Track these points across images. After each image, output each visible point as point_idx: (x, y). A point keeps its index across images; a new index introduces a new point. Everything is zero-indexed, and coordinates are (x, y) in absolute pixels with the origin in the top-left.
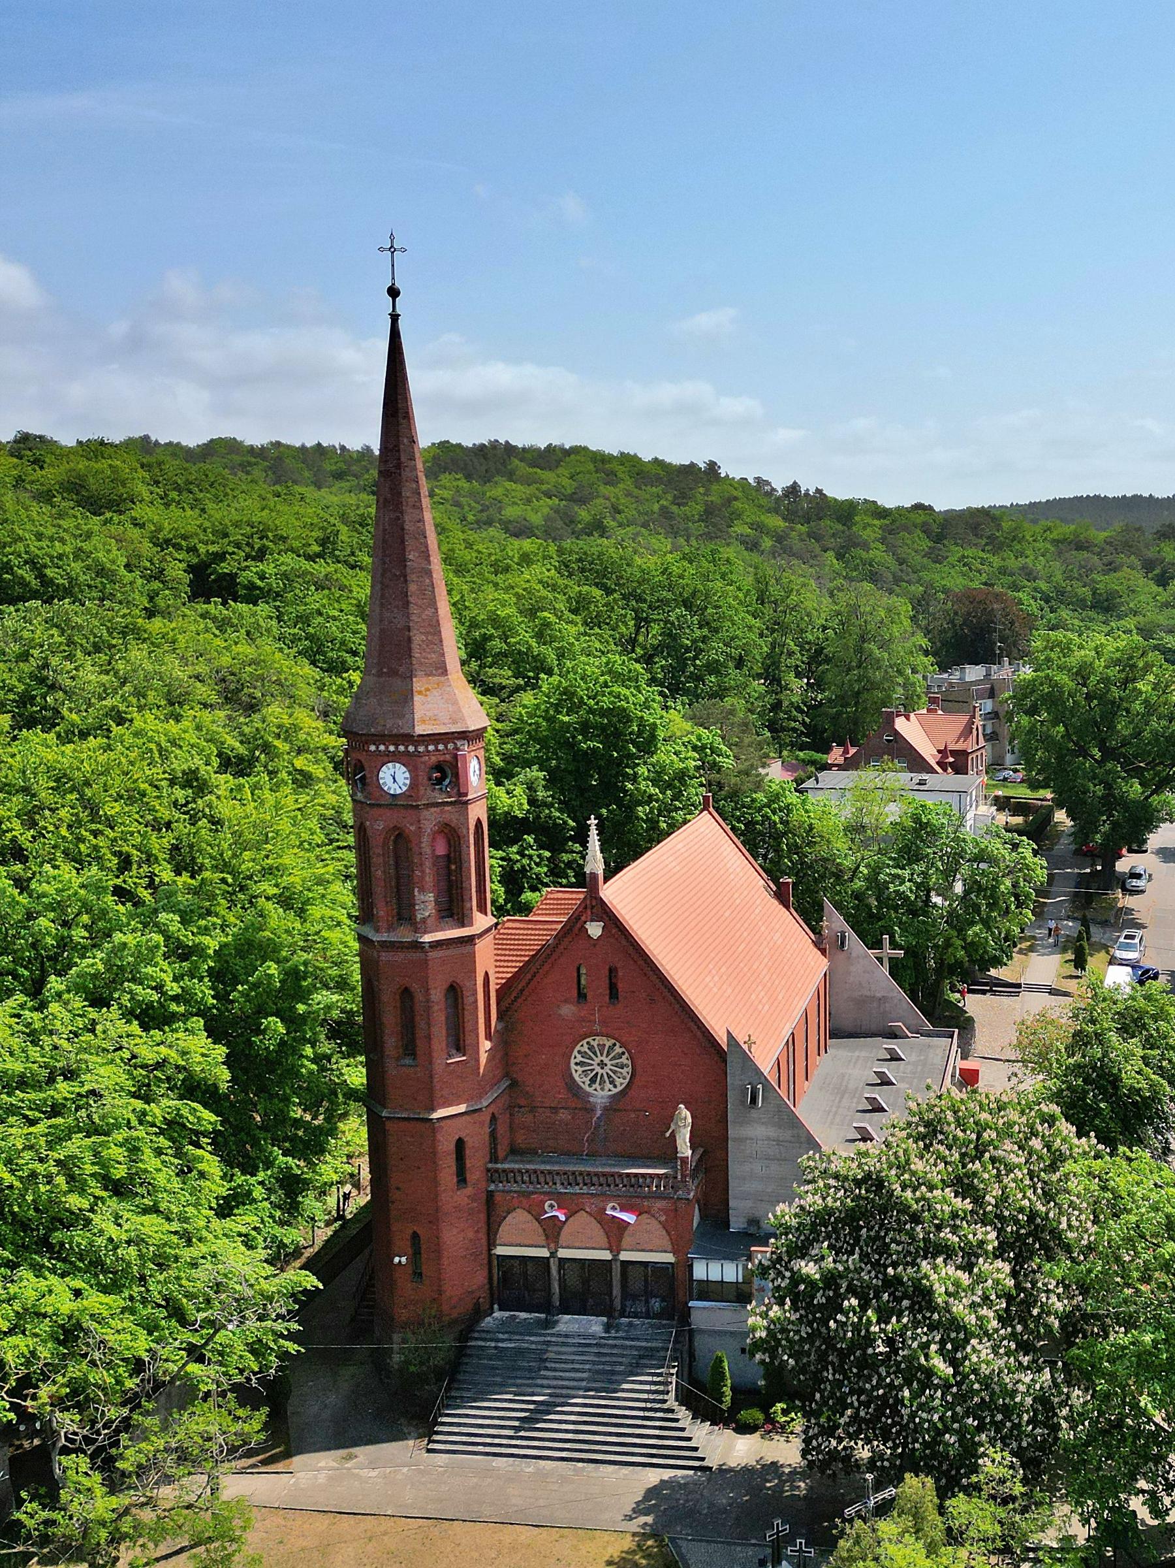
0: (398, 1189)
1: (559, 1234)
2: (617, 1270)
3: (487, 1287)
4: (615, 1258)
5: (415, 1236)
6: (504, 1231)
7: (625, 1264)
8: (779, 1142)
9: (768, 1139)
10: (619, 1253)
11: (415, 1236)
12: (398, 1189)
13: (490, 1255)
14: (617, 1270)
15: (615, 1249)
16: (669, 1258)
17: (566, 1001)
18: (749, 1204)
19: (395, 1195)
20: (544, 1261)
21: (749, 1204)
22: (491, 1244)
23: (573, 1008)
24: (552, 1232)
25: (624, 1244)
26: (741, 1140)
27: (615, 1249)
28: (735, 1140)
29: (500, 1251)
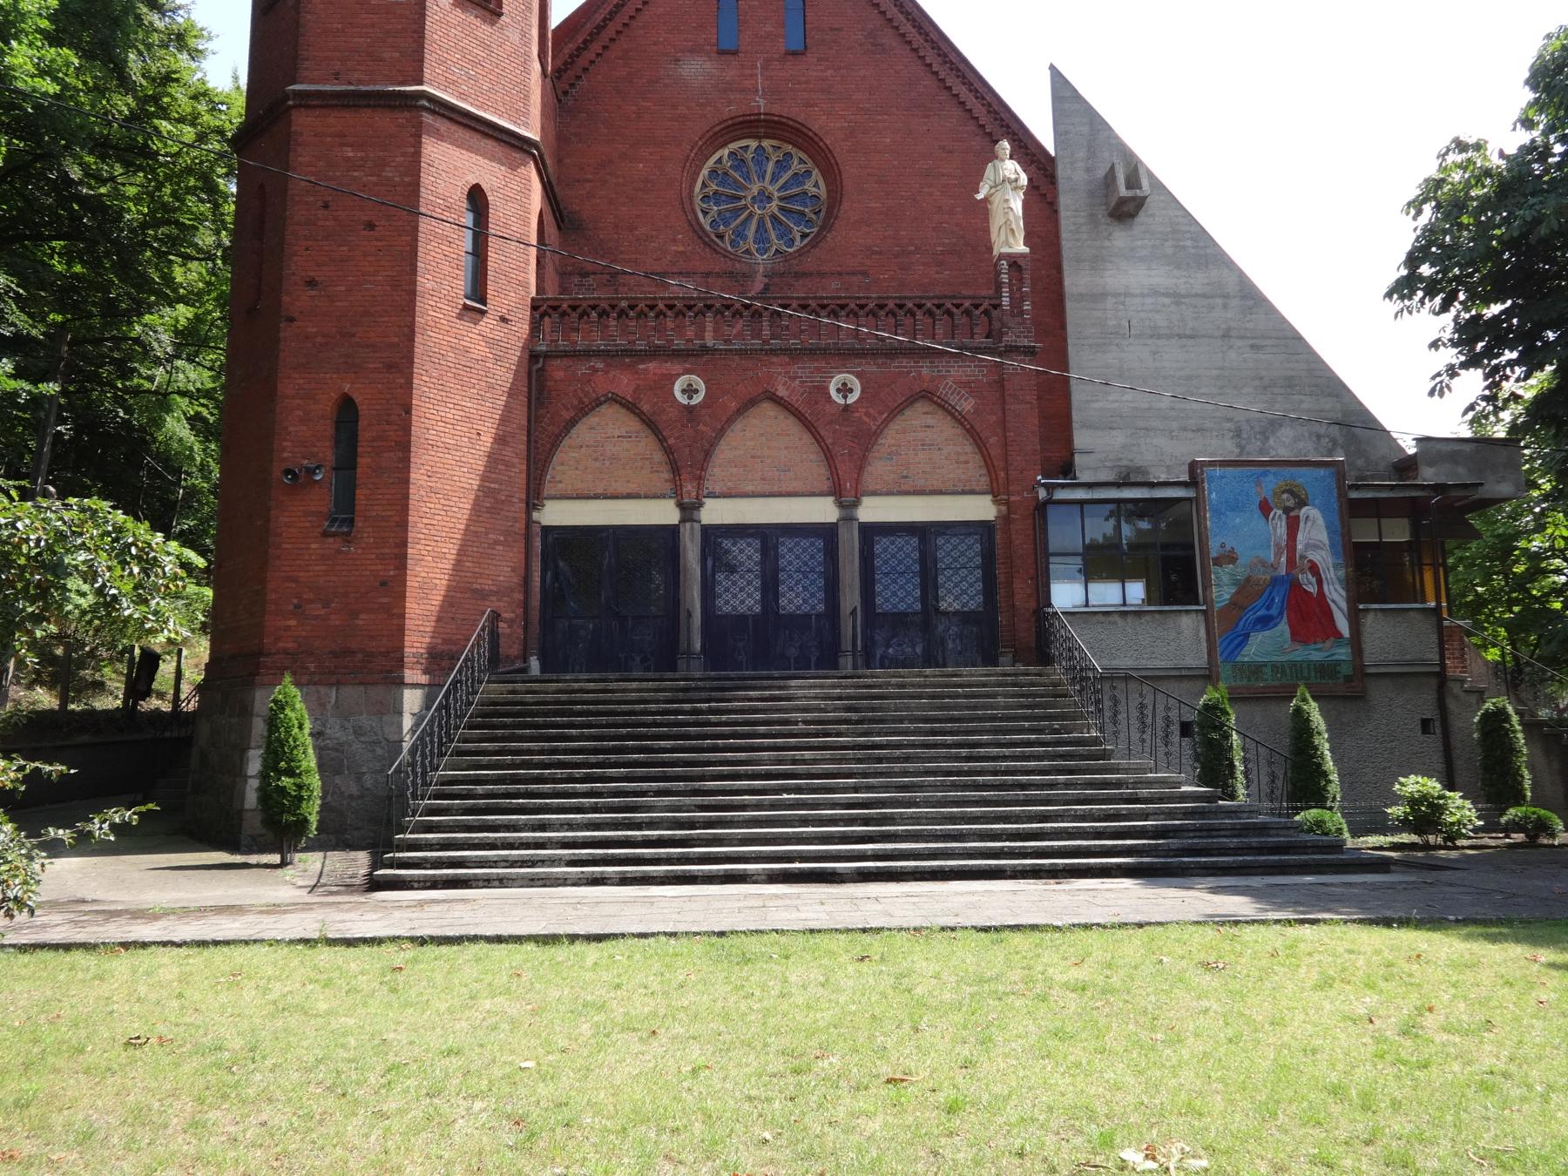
0: (311, 283)
1: (708, 454)
2: (850, 545)
3: (519, 596)
4: (848, 518)
5: (347, 409)
6: (566, 464)
7: (871, 531)
8: (1177, 297)
9: (1155, 293)
10: (856, 504)
11: (347, 409)
12: (311, 283)
13: (529, 522)
14: (850, 545)
15: (846, 494)
16: (981, 508)
17: (695, 50)
18: (1118, 439)
19: (298, 299)
20: (669, 534)
21: (1118, 439)
22: (534, 497)
23: (708, 65)
24: (686, 459)
25: (869, 480)
26: (1099, 297)
27: (846, 494)
28: (1081, 297)
29: (556, 514)
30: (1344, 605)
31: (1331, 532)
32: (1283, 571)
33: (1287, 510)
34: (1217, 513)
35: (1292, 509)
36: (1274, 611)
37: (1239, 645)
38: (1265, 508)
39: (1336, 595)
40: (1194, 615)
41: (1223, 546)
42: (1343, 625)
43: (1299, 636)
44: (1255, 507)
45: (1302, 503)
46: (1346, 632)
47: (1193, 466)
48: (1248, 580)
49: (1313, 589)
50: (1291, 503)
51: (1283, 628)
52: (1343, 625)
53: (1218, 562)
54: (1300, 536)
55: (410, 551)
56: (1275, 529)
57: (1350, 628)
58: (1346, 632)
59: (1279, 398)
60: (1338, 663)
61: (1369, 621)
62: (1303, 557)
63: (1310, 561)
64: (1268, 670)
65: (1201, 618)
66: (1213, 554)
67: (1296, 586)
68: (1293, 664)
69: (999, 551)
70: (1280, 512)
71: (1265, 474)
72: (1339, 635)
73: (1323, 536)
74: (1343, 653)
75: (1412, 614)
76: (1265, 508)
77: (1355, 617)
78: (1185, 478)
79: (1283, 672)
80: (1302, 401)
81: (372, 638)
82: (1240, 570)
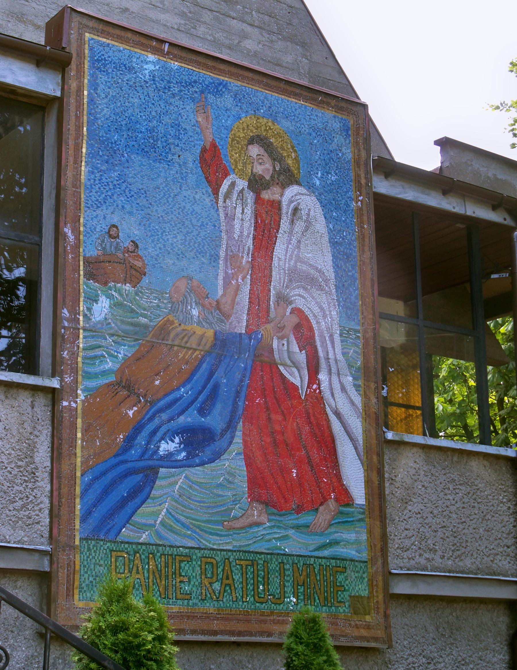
30: (357, 425)
31: (340, 257)
32: (240, 323)
33: (256, 184)
34: (107, 151)
35: (267, 186)
36: (215, 420)
37: (133, 493)
38: (213, 165)
39: (345, 403)
40: (24, 399)
41: (112, 232)
42: (354, 475)
43: (266, 489)
44: (191, 158)
45: (287, 177)
46: (359, 493)
47: (56, 27)
48: (163, 330)
49: (297, 378)
50: (264, 168)
51: (233, 463)
52: (354, 475)
53: (97, 270)
54: (280, 249)
55: (364, 492)
56: (230, 218)
57: (368, 482)
58: (359, 493)
59: (207, 16)
60: (341, 564)
61: (406, 468)
62: (283, 299)
63: (298, 312)
64: (192, 570)
65: (41, 408)
66: (90, 250)
67: (266, 366)
68: (250, 560)
69: (271, 552)
70: (242, 184)
71: (218, 89)
72: (344, 497)
73: (321, 259)
74: (353, 542)
75: (474, 464)
76: (213, 165)
77: (378, 454)
78: (37, 37)
79: (228, 583)
80: (245, 36)
81: (485, 466)
82: (150, 303)
